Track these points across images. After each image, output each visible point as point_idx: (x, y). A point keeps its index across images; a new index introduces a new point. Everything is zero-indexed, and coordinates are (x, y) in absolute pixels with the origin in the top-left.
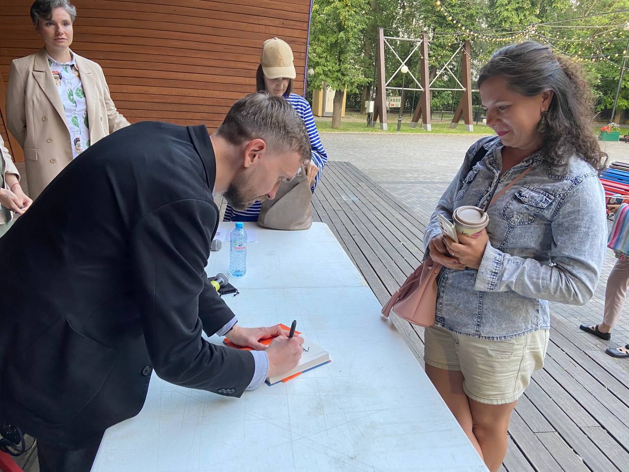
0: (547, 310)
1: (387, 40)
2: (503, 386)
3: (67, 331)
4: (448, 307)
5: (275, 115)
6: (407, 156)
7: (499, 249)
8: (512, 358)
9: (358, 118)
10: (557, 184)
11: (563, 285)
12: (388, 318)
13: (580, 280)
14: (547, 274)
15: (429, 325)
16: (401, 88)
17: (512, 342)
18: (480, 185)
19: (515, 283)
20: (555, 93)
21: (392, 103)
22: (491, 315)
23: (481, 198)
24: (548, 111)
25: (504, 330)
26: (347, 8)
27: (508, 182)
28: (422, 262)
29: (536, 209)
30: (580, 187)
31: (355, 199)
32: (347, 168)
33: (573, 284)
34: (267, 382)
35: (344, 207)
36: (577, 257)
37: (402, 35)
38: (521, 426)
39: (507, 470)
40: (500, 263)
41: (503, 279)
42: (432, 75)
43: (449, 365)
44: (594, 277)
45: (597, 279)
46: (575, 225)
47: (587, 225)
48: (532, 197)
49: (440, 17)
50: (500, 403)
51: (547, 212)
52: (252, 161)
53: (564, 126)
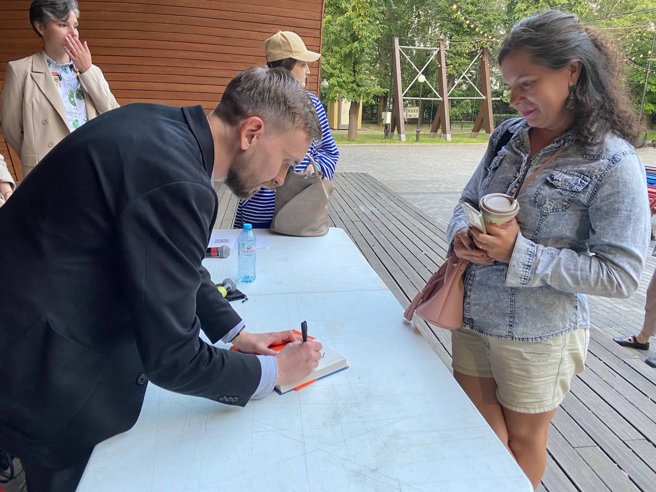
0: (586, 306)
1: (403, 49)
2: (541, 392)
3: (48, 333)
4: (477, 307)
5: (273, 88)
6: (427, 166)
7: (531, 240)
8: (549, 361)
9: (375, 129)
10: (593, 164)
11: (605, 276)
12: (412, 321)
13: (622, 269)
14: (586, 264)
15: (456, 328)
16: (419, 98)
17: (548, 343)
18: (507, 172)
19: (551, 276)
20: (583, 64)
21: (409, 114)
22: (524, 314)
23: (509, 186)
24: (577, 85)
25: (539, 330)
26: (361, 18)
27: (538, 166)
28: (446, 260)
29: (570, 194)
30: (618, 165)
31: (373, 209)
32: (364, 179)
33: (616, 275)
34: (277, 390)
35: (362, 217)
36: (618, 243)
37: (418, 44)
38: (559, 441)
39: (547, 490)
40: (533, 255)
41: (537, 272)
42: (450, 84)
43: (479, 372)
44: (639, 266)
45: (643, 267)
46: (615, 209)
47: (629, 208)
48: (566, 181)
49: (456, 24)
50: (538, 411)
51: (583, 196)
52: (250, 143)
53: (595, 99)
